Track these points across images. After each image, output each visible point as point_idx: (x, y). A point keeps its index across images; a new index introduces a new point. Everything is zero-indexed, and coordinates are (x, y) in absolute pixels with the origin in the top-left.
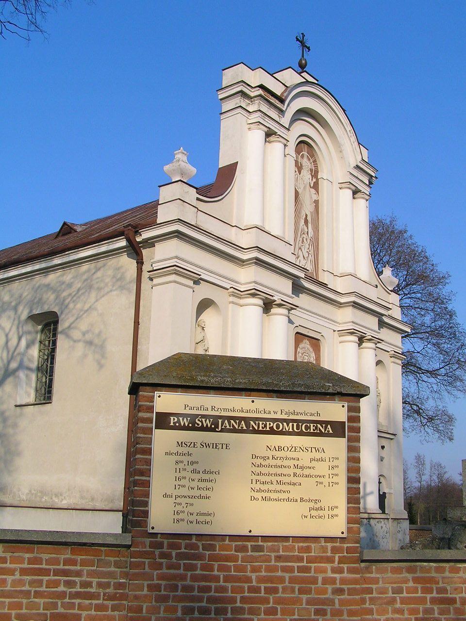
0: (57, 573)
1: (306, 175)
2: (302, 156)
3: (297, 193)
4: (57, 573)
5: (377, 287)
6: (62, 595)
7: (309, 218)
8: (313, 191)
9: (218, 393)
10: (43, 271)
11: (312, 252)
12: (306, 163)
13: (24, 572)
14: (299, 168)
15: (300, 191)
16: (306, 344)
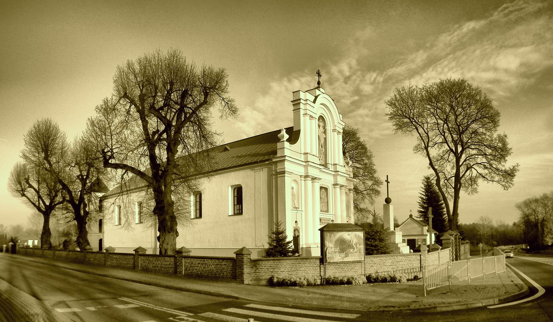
0: (314, 263)
1: (321, 128)
2: (320, 122)
3: (319, 136)
4: (314, 263)
5: (345, 166)
6: (315, 266)
7: (323, 145)
8: (324, 134)
9: (475, 257)
10: (274, 189)
11: (324, 157)
12: (322, 124)
13: (308, 263)
14: (319, 126)
15: (319, 135)
16: (323, 190)
